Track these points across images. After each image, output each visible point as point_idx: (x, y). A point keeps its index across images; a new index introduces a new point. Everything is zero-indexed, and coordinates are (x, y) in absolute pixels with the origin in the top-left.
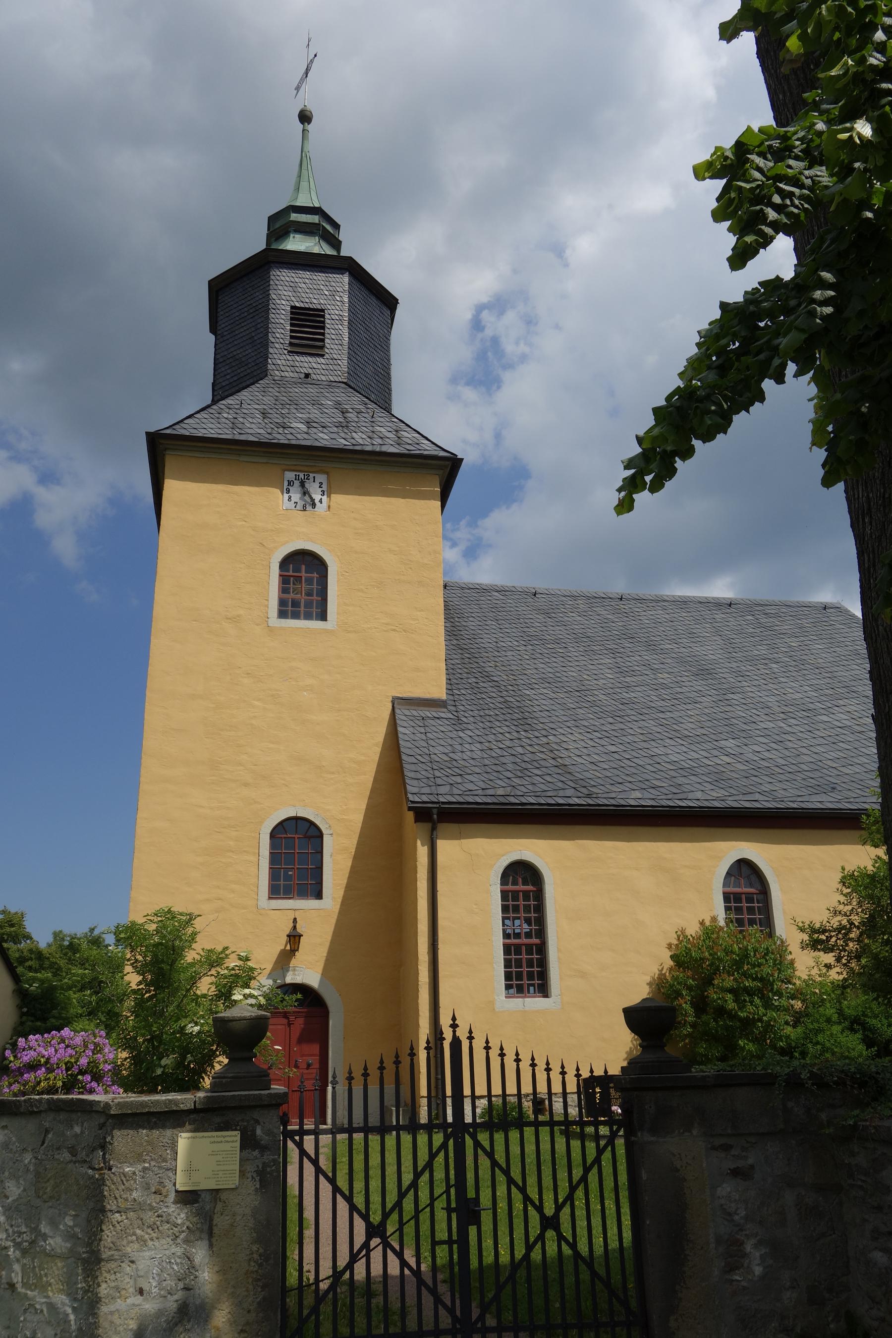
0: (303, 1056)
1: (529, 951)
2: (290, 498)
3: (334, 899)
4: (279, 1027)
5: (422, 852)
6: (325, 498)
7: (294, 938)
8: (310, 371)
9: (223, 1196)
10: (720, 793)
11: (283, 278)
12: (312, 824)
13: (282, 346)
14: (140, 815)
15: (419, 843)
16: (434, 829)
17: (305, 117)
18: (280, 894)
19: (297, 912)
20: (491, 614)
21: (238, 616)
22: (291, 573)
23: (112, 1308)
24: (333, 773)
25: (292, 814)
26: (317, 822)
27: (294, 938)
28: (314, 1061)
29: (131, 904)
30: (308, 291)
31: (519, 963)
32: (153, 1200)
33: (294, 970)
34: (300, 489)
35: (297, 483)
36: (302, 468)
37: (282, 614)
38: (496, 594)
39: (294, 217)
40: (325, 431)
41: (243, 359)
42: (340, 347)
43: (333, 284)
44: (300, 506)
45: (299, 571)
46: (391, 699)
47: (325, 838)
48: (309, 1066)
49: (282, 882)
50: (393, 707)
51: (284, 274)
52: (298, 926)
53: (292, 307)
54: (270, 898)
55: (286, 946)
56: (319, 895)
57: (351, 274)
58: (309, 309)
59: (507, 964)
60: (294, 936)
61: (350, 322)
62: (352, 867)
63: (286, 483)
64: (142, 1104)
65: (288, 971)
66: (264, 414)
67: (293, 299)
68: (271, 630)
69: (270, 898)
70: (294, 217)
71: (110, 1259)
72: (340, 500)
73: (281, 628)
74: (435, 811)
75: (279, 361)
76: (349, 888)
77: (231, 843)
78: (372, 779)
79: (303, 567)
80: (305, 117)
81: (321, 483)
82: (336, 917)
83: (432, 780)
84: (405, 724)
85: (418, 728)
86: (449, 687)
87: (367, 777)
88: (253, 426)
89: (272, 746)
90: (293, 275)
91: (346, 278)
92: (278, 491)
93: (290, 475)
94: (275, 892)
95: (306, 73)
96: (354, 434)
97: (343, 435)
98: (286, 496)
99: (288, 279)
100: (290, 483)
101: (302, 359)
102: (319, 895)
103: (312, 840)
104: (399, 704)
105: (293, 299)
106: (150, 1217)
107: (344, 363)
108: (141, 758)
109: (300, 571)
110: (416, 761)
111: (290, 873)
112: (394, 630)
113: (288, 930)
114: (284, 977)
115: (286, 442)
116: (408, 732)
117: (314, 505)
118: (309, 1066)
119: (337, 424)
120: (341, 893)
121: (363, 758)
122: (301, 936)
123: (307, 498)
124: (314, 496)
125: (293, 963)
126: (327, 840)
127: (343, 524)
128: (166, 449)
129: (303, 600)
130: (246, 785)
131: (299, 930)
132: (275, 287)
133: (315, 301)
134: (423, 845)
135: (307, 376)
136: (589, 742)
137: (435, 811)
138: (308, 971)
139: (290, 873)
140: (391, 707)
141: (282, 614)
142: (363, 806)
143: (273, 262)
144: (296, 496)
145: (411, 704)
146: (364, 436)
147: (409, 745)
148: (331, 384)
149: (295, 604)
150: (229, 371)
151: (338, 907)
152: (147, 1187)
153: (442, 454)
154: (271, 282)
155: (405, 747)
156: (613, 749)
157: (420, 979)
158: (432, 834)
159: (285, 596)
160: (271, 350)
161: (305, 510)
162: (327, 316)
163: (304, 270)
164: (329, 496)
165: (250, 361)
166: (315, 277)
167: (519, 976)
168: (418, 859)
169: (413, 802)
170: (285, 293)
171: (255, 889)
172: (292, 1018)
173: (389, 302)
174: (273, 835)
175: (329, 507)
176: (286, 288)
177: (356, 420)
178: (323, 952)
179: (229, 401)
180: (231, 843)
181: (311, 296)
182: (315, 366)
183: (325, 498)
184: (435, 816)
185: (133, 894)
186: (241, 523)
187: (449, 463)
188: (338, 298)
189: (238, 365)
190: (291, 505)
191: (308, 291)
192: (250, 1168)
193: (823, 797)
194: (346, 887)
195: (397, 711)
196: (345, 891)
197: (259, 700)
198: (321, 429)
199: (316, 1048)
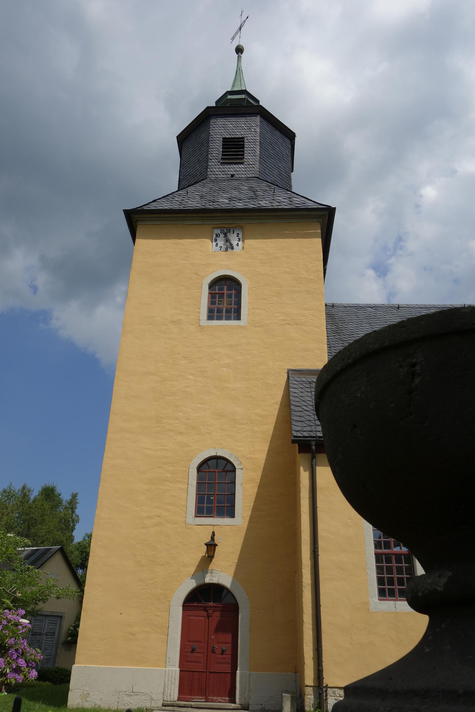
0: (218, 643)
1: (398, 560)
2: (217, 244)
3: (243, 517)
4: (201, 618)
5: (304, 476)
6: (240, 243)
7: (211, 546)
8: (235, 173)
11: (218, 123)
12: (228, 461)
13: (216, 161)
14: (106, 455)
15: (302, 469)
16: (313, 457)
18: (204, 514)
19: (215, 527)
20: (366, 320)
21: (180, 320)
22: (217, 291)
24: (244, 424)
25: (213, 454)
26: (231, 460)
27: (211, 546)
28: (227, 647)
29: (96, 519)
30: (233, 128)
31: (390, 570)
33: (212, 573)
37: (210, 317)
38: (370, 309)
39: (229, 97)
40: (241, 201)
42: (254, 157)
43: (250, 123)
44: (223, 248)
45: (223, 290)
46: (286, 371)
47: (237, 471)
48: (223, 652)
49: (205, 505)
50: (288, 376)
51: (219, 121)
52: (215, 538)
53: (223, 138)
54: (196, 516)
55: (206, 554)
56: (232, 515)
57: (261, 116)
58: (235, 138)
59: (379, 570)
60: (211, 545)
61: (260, 143)
62: (258, 493)
63: (214, 236)
65: (207, 573)
66: (201, 197)
67: (224, 134)
70: (229, 97)
72: (249, 242)
73: (209, 327)
74: (313, 443)
75: (215, 170)
76: (255, 509)
77: (168, 475)
78: (273, 428)
79: (225, 287)
80: (239, 50)
81: (238, 234)
82: (245, 532)
83: (313, 422)
84: (296, 386)
85: (306, 389)
86: (330, 351)
87: (268, 428)
88: (193, 203)
89: (200, 406)
90: (225, 121)
91: (258, 119)
92: (209, 241)
93: (218, 231)
94: (201, 511)
95: (240, 29)
96: (260, 202)
97: (253, 203)
98: (214, 243)
99: (221, 123)
100: (217, 235)
101: (229, 166)
102: (232, 515)
103: (228, 473)
104: (292, 374)
105: (224, 134)
107: (257, 166)
108: (109, 416)
109: (223, 290)
110: (302, 410)
111: (212, 498)
112: (289, 324)
113: (208, 539)
114: (204, 578)
116: (297, 391)
117: (232, 248)
118: (223, 652)
119: (249, 198)
120: (249, 513)
121: (266, 413)
123: (228, 244)
124: (232, 242)
125: (211, 567)
126: (239, 473)
127: (252, 258)
128: (137, 221)
129: (225, 309)
130: (181, 433)
131: (216, 542)
132: (213, 129)
134: (305, 471)
135: (232, 176)
137: (313, 443)
138: (222, 574)
139: (212, 498)
140: (286, 377)
141: (210, 317)
142: (266, 447)
144: (221, 242)
145: (301, 374)
146: (267, 202)
147: (297, 399)
148: (248, 179)
149: (219, 311)
151: (247, 524)
154: (211, 126)
155: (294, 401)
157: (304, 581)
158: (312, 462)
159: (213, 306)
160: (210, 164)
161: (227, 251)
162: (246, 141)
163: (232, 117)
164: (243, 241)
166: (238, 120)
167: (391, 582)
168: (301, 482)
169: (295, 437)
170: (219, 131)
171: (185, 509)
172: (210, 611)
173: (290, 136)
174: (200, 468)
175: (243, 248)
176: (220, 128)
177: (263, 194)
178: (235, 559)
180: (168, 475)
181: (236, 131)
182: (237, 169)
183: (240, 243)
184: (314, 447)
185: (98, 512)
186: (183, 262)
187: (326, 213)
188: (253, 130)
189: (191, 175)
190: (218, 248)
191: (233, 128)
194: (253, 509)
195: (291, 378)
196: (252, 512)
197: (192, 374)
198: (238, 201)
199: (228, 637)
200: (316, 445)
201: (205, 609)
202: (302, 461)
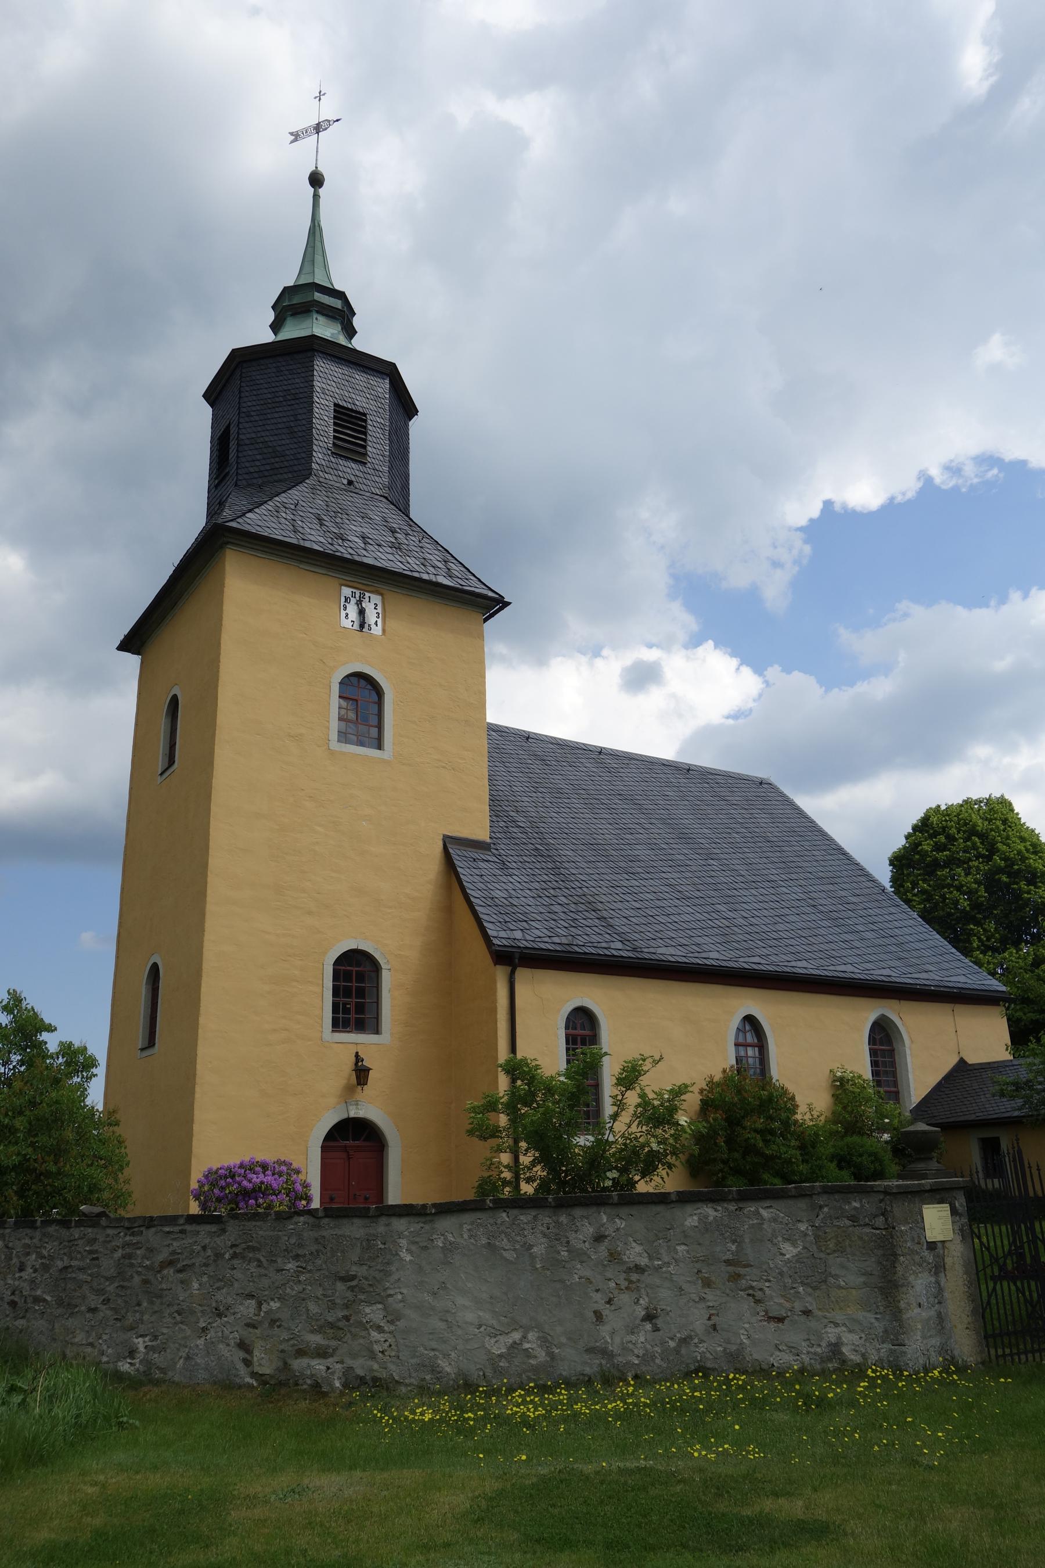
2: (347, 615)
8: (353, 479)
9: (947, 1245)
10: (729, 955)
17: (316, 180)
23: (908, 1316)
32: (916, 1247)
34: (356, 607)
35: (353, 601)
36: (360, 586)
39: (318, 296)
41: (279, 448)
58: (351, 410)
63: (343, 599)
64: (907, 1186)
68: (332, 753)
69: (333, 1031)
70: (318, 296)
71: (903, 1286)
74: (517, 956)
80: (316, 180)
93: (347, 591)
94: (338, 1024)
106: (917, 1258)
115: (349, 556)
122: (369, 1070)
128: (228, 543)
130: (310, 913)
133: (361, 403)
136: (518, 885)
137: (517, 956)
138: (370, 1107)
143: (317, 351)
150: (258, 457)
152: (913, 1240)
153: (491, 594)
156: (638, 906)
165: (287, 452)
179: (282, 498)
192: (957, 1228)
193: (804, 964)
200: (520, 959)
201: (345, 1149)
202: (501, 975)
